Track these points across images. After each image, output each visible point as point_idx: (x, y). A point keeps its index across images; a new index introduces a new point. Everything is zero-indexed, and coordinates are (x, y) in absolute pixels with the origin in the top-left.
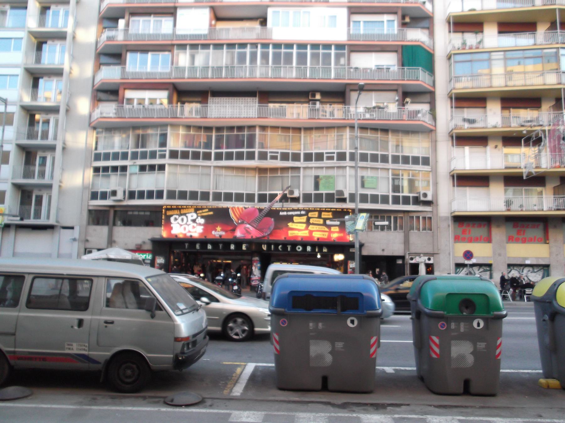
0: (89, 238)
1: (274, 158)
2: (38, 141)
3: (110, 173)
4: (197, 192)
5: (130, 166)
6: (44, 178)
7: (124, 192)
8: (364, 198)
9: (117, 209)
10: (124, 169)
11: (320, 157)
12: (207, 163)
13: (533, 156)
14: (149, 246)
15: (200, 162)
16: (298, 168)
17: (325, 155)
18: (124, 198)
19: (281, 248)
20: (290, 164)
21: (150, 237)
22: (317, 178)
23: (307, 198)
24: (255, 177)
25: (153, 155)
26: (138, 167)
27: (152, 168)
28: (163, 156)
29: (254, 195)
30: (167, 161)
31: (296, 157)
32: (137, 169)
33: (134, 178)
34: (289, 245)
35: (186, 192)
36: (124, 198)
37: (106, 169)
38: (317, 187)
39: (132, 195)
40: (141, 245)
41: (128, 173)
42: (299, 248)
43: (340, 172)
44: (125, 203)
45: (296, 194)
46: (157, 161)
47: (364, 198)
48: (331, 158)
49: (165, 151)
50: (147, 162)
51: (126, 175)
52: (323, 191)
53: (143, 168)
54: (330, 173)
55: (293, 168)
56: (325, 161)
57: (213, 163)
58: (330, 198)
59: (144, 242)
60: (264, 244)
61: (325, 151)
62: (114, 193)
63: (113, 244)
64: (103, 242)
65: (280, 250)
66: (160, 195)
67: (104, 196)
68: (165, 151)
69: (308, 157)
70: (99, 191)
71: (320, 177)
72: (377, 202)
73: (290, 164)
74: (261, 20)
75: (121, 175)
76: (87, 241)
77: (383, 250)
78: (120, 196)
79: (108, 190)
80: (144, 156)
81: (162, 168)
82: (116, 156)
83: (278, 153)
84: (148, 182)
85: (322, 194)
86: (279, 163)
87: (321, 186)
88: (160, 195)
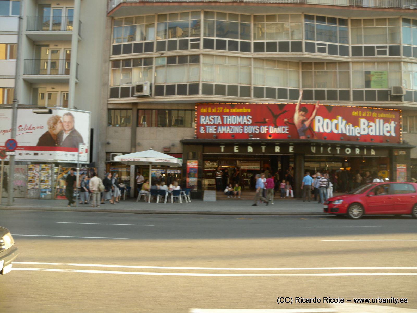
0: (110, 141)
1: (322, 50)
2: (49, 32)
3: (132, 67)
4: (236, 87)
5: (156, 57)
9: (140, 107)
11: (370, 51)
12: (245, 55)
13: (275, 128)
14: (178, 149)
15: (239, 54)
16: (348, 63)
17: (376, 49)
19: (330, 150)
20: (338, 58)
21: (180, 139)
22: (367, 73)
23: (358, 95)
24: (298, 72)
25: (184, 45)
26: (166, 59)
27: (183, 60)
28: (196, 46)
30: (202, 50)
31: (344, 51)
32: (165, 62)
35: (224, 86)
36: (151, 94)
37: (127, 62)
38: (368, 84)
40: (169, 148)
41: (154, 66)
42: (348, 151)
43: (395, 67)
46: (190, 52)
48: (384, 53)
49: (199, 40)
50: (177, 52)
51: (151, 68)
52: (375, 88)
53: (171, 60)
54: (382, 68)
55: (341, 63)
56: (376, 56)
57: (252, 54)
58: (384, 95)
59: (173, 145)
60: (313, 146)
61: (375, 45)
62: (140, 88)
63: (138, 148)
64: (126, 144)
65: (330, 152)
67: (125, 92)
68: (199, 40)
69: (357, 51)
71: (372, 73)
73: (338, 58)
75: (145, 68)
76: (108, 143)
79: (130, 86)
80: (172, 45)
83: (325, 45)
84: (179, 75)
85: (375, 91)
87: (372, 83)
88: (194, 89)
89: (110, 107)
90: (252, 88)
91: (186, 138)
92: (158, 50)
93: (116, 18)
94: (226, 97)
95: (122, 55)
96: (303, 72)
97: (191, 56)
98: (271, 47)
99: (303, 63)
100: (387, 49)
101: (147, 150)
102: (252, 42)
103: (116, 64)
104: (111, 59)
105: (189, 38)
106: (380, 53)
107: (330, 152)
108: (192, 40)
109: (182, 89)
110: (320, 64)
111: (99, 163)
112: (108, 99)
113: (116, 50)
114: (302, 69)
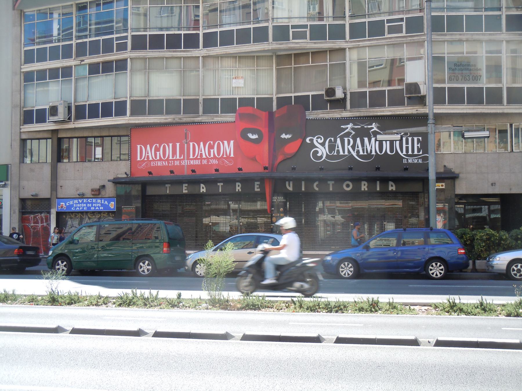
6: (425, 105)
7: (69, 108)
8: (456, 96)
10: (67, 72)
14: (110, 190)
16: (344, 49)
18: (70, 118)
23: (358, 99)
25: (108, 47)
27: (107, 67)
28: (122, 47)
29: (272, 99)
33: (83, 84)
34: (331, 180)
39: (81, 112)
42: (348, 186)
44: (71, 125)
45: (339, 94)
47: (456, 96)
49: (126, 38)
53: (94, 69)
55: (332, 51)
56: (387, 35)
62: (54, 110)
65: (317, 189)
66: (120, 109)
70: (485, 87)
72: (462, 102)
74: (182, 270)
77: (511, 189)
78: (61, 114)
81: (121, 65)
82: (54, 54)
84: (101, 90)
86: (308, 44)
88: (120, 109)
89: (24, 137)
90: (201, 101)
91: (120, 176)
92: (77, 56)
93: (25, 11)
94: (383, 42)
95: (36, 64)
96: (278, 70)
97: (117, 61)
98: (227, 38)
99: (278, 57)
100: (404, 24)
101: (177, 195)
102: (201, 33)
103: (28, 77)
104: (22, 70)
105: (115, 36)
106: (392, 30)
107: (317, 189)
108: (118, 39)
109: (107, 110)
110: (300, 55)
111: (222, 271)
112: (20, 126)
113: (29, 58)
114: (278, 64)
